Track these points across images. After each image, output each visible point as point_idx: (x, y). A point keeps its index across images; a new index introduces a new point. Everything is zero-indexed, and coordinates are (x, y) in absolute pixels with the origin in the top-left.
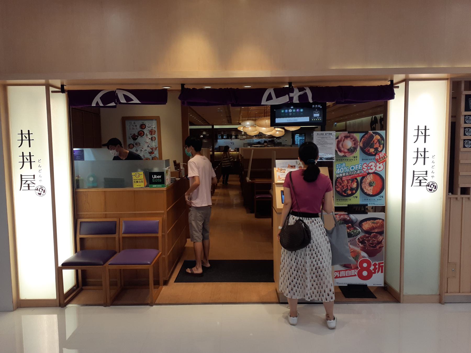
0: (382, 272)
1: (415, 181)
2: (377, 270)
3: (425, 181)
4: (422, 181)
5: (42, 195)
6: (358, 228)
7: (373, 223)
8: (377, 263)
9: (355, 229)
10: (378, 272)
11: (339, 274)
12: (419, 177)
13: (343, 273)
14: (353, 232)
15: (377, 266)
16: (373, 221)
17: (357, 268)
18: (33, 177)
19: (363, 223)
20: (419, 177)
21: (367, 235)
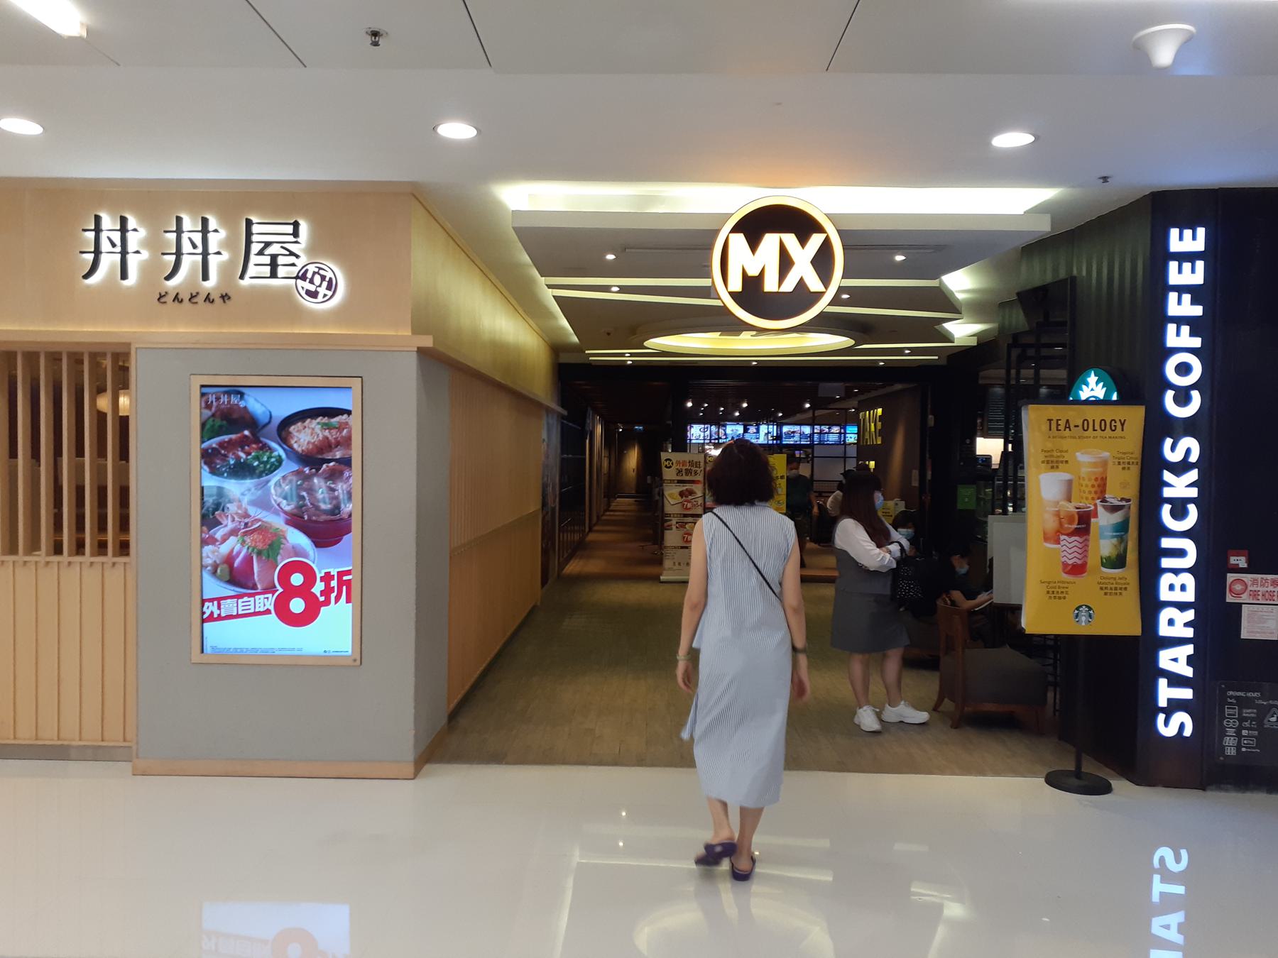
0: (348, 601)
1: (254, 259)
2: (333, 596)
3: (292, 259)
4: (281, 260)
5: (320, 298)
6: (274, 445)
7: (327, 427)
8: (334, 572)
9: (265, 447)
10: (338, 599)
11: (219, 608)
12: (268, 244)
13: (229, 607)
14: (257, 458)
15: (334, 583)
16: (325, 420)
17: (270, 589)
18: (290, 229)
19: (292, 429)
20: (268, 244)
21: (307, 470)
